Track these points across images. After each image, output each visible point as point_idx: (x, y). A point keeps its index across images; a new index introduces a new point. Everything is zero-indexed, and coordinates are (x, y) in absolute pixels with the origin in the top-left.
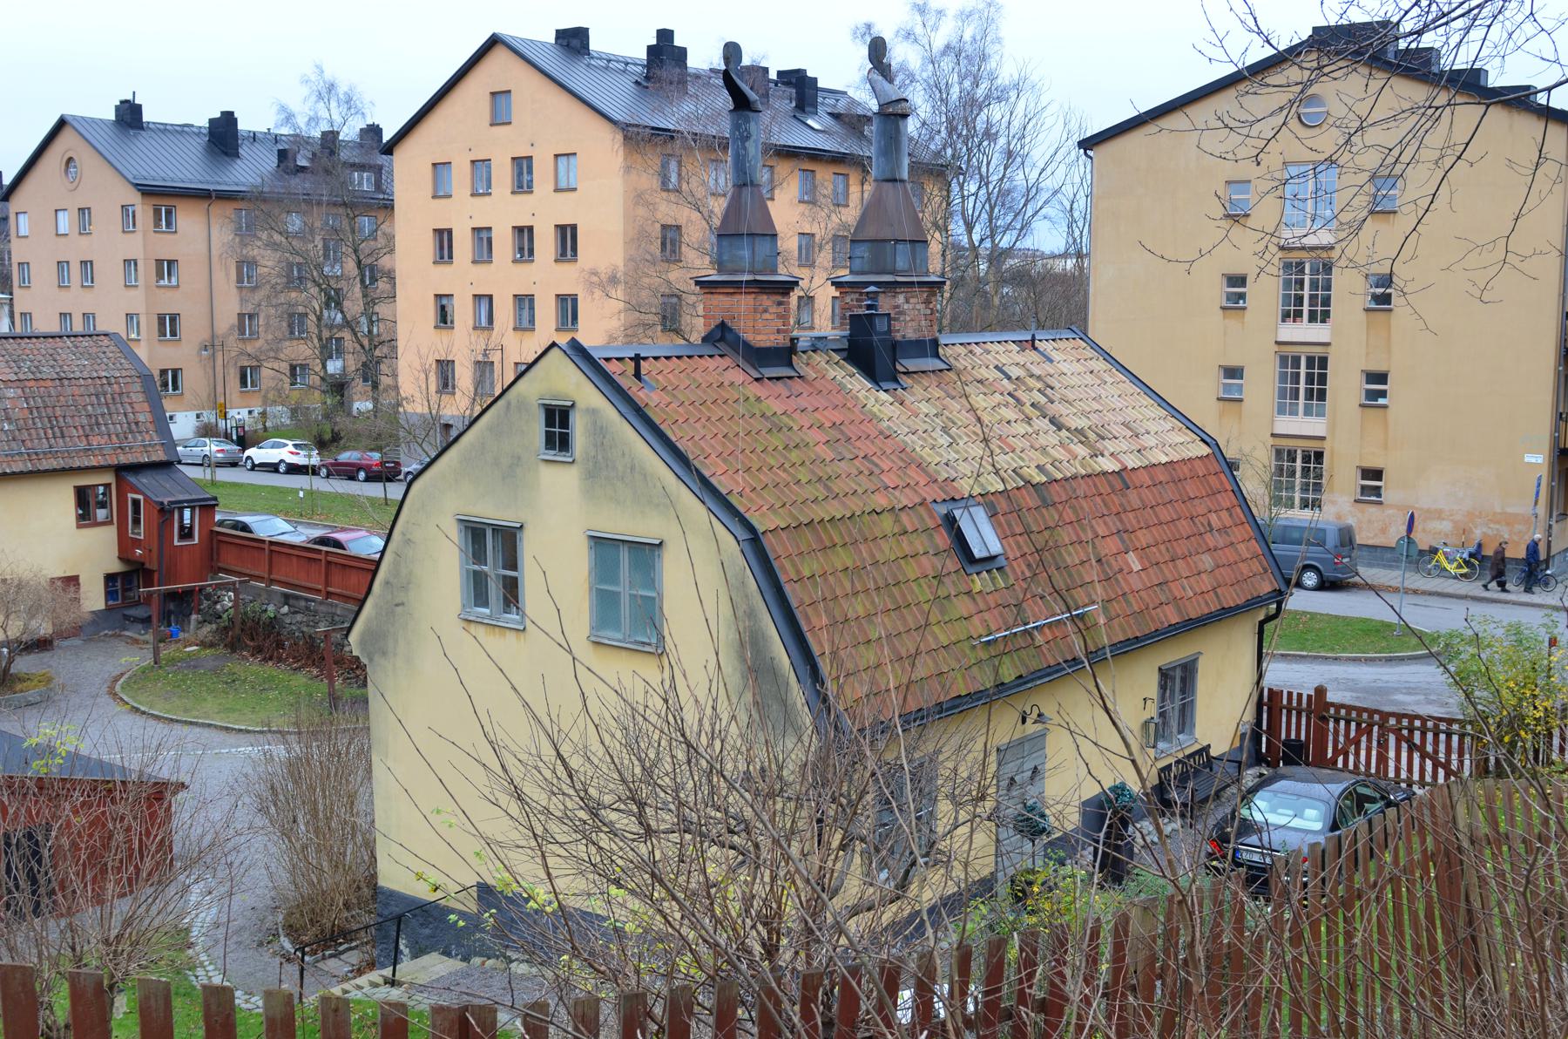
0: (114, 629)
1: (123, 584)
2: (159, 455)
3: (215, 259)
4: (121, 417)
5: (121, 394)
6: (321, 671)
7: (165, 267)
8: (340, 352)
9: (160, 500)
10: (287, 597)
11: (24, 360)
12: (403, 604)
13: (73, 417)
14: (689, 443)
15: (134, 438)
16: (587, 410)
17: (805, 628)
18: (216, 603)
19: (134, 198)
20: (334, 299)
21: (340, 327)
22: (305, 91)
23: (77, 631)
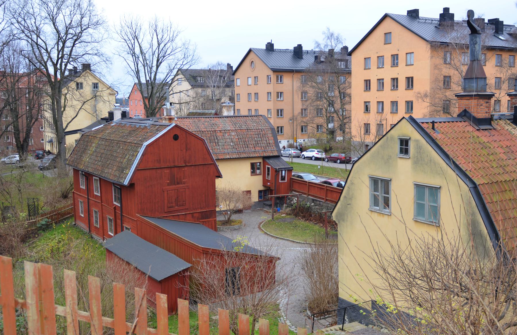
2: (276, 154)
3: (294, 92)
4: (265, 142)
5: (265, 134)
6: (323, 225)
7: (280, 94)
8: (333, 121)
10: (313, 200)
11: (237, 124)
12: (350, 204)
13: (251, 141)
14: (452, 152)
15: (269, 148)
16: (415, 140)
17: (494, 220)
18: (291, 201)
19: (271, 73)
20: (331, 104)
21: (333, 113)
22: (324, 36)
23: (249, 208)
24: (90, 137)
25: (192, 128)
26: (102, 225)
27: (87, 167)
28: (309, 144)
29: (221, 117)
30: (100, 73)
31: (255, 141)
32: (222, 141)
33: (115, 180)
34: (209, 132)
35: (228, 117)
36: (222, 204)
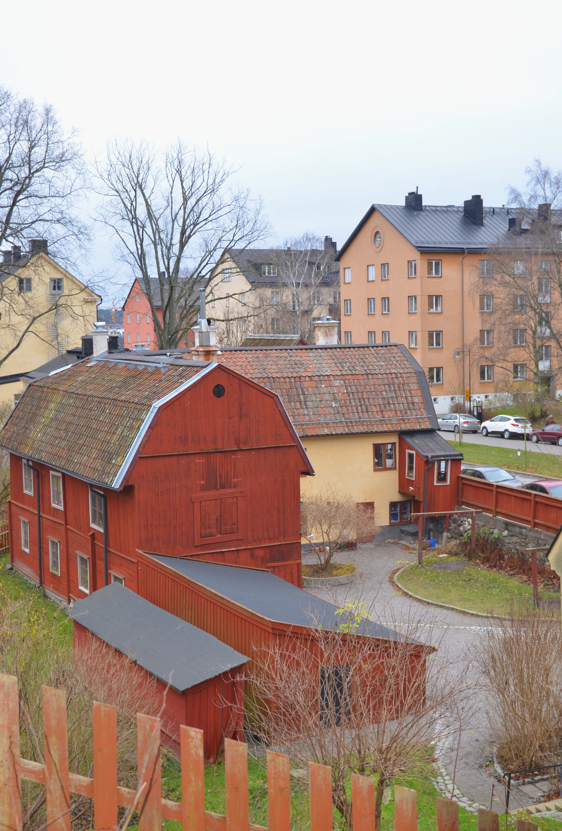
0: (395, 538)
1: (401, 510)
2: (426, 425)
5: (404, 384)
6: (529, 578)
8: (548, 356)
9: (426, 454)
10: (507, 524)
18: (460, 526)
19: (416, 256)
22: (528, 178)
23: (371, 538)
24: (45, 390)
25: (251, 371)
26: (65, 571)
27: (39, 451)
28: (498, 405)
29: (311, 349)
30: (67, 258)
31: (384, 398)
32: (314, 398)
33: (93, 477)
34: (288, 380)
35: (326, 349)
36: (313, 530)
